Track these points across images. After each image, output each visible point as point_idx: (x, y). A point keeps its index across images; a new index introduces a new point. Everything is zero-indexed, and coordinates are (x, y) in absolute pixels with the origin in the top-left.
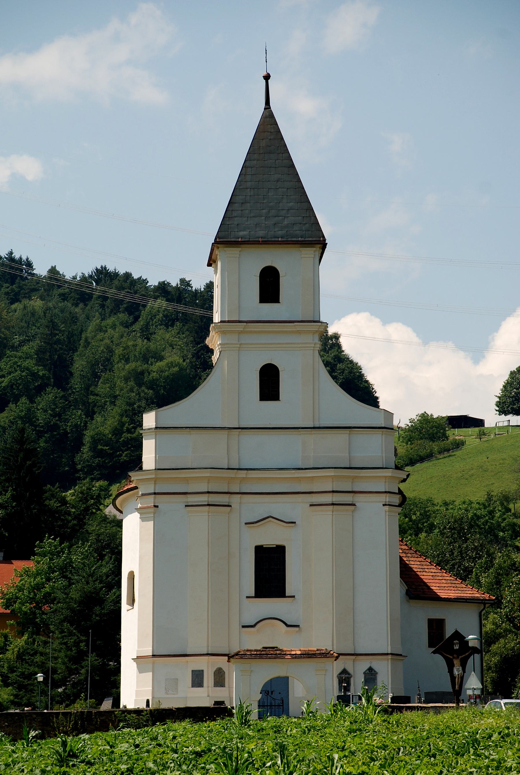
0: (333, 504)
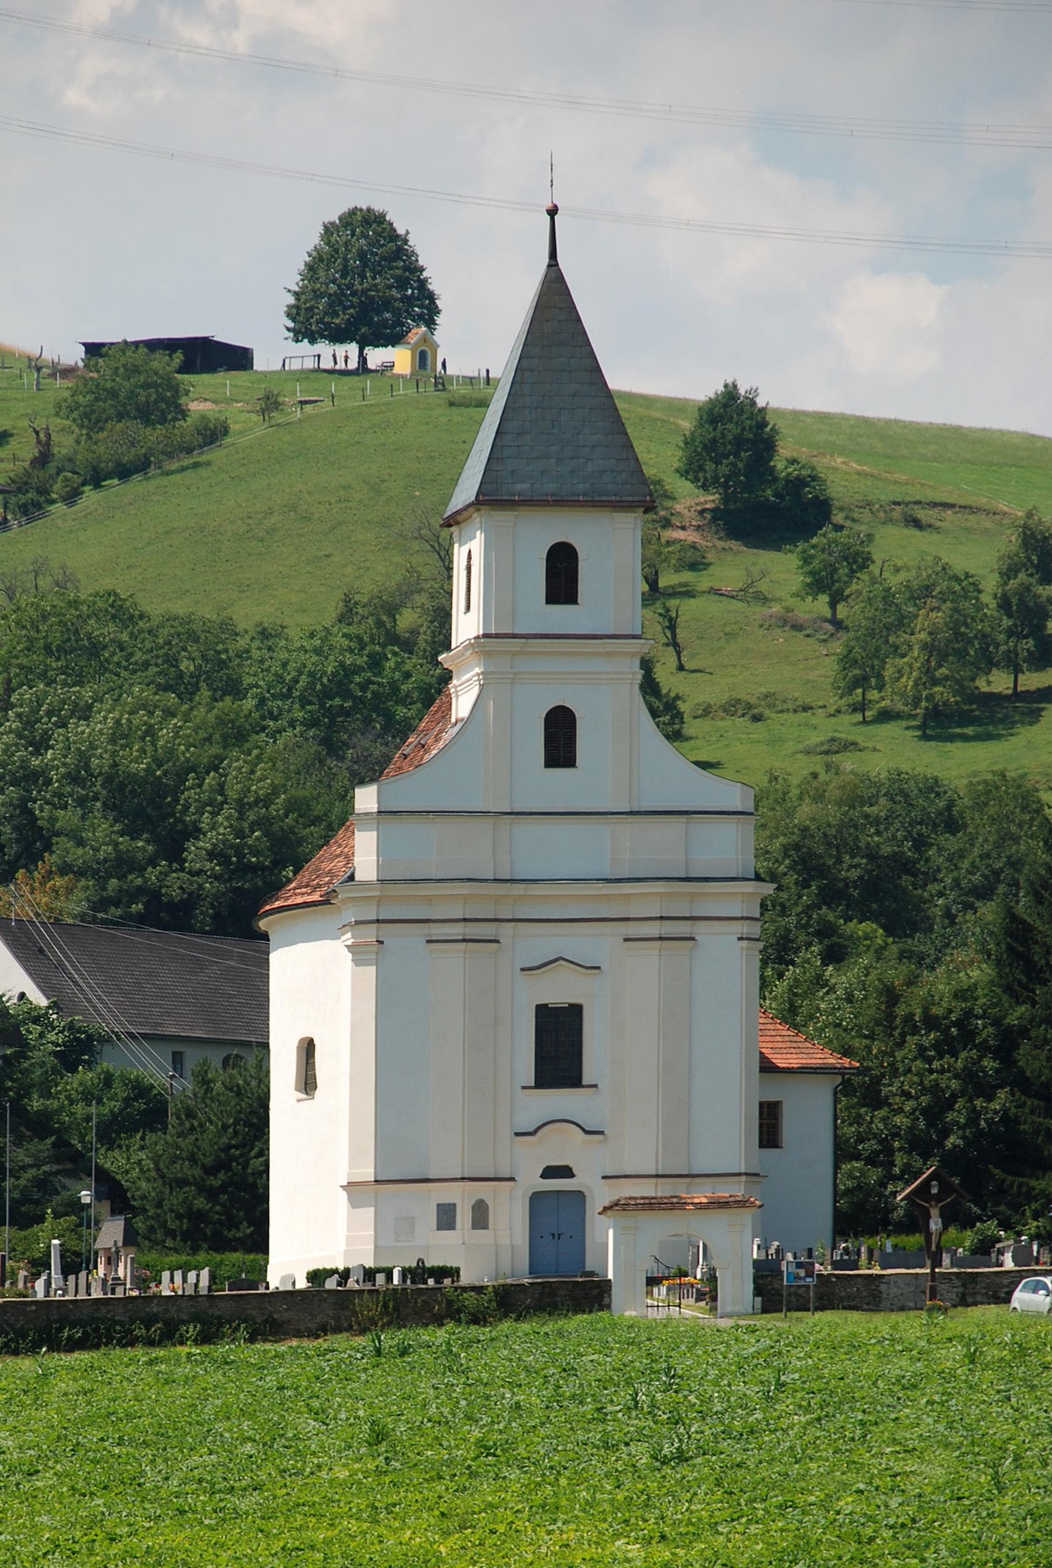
0: (661, 939)
